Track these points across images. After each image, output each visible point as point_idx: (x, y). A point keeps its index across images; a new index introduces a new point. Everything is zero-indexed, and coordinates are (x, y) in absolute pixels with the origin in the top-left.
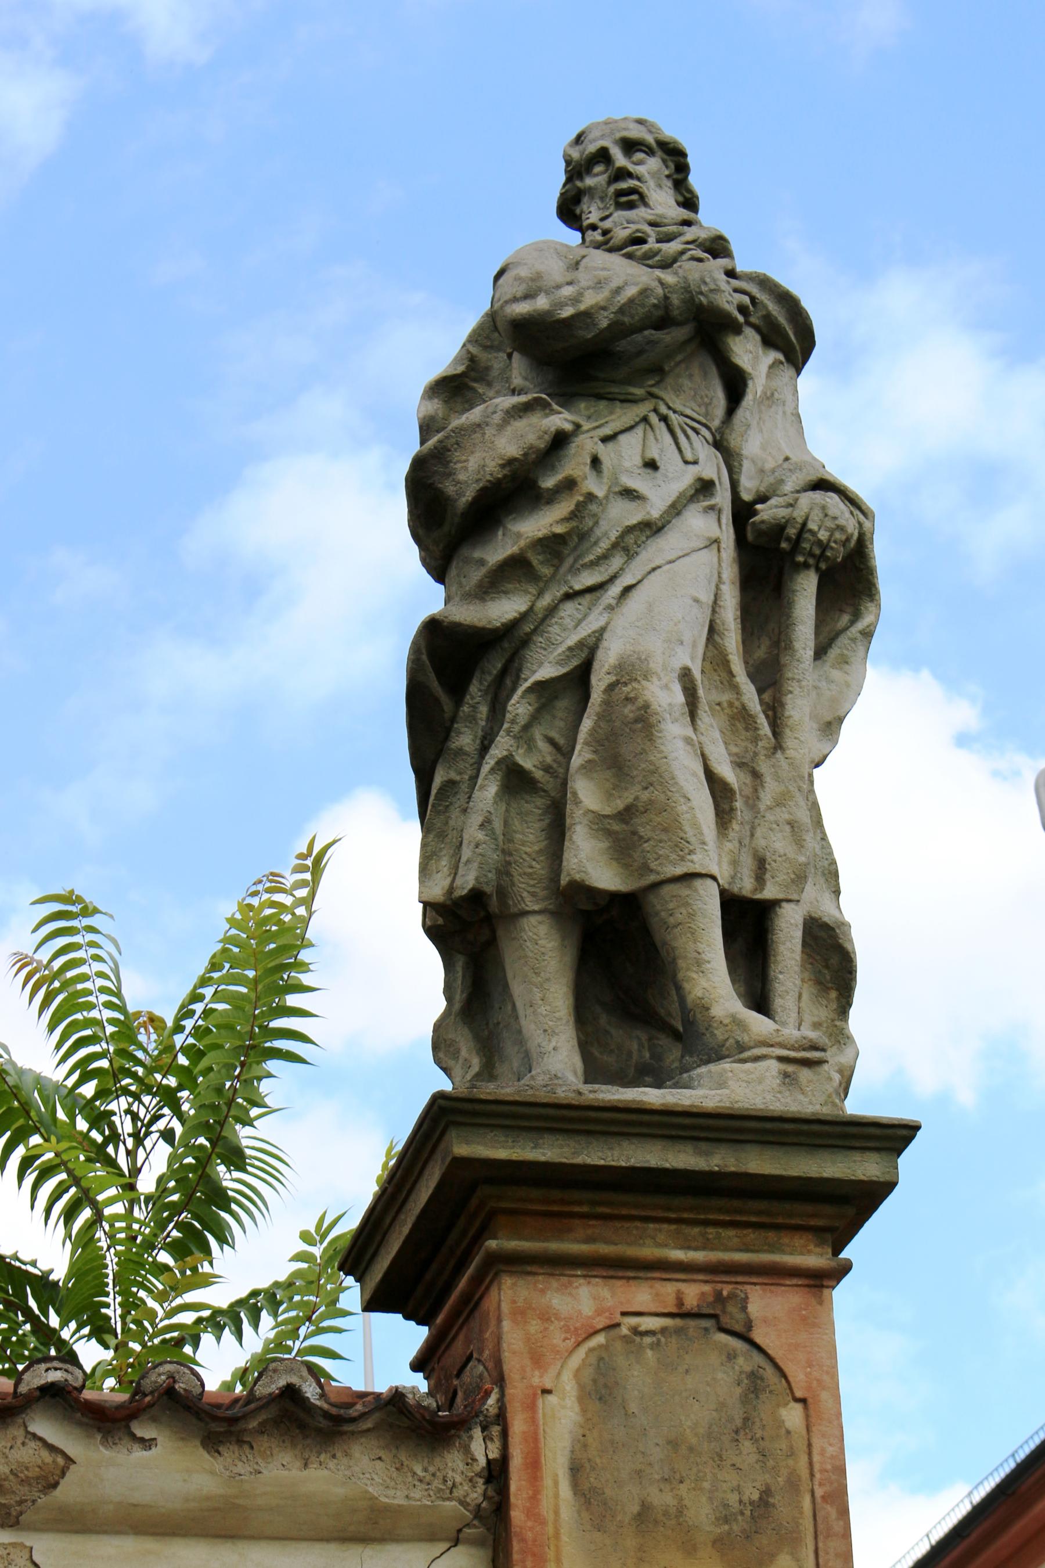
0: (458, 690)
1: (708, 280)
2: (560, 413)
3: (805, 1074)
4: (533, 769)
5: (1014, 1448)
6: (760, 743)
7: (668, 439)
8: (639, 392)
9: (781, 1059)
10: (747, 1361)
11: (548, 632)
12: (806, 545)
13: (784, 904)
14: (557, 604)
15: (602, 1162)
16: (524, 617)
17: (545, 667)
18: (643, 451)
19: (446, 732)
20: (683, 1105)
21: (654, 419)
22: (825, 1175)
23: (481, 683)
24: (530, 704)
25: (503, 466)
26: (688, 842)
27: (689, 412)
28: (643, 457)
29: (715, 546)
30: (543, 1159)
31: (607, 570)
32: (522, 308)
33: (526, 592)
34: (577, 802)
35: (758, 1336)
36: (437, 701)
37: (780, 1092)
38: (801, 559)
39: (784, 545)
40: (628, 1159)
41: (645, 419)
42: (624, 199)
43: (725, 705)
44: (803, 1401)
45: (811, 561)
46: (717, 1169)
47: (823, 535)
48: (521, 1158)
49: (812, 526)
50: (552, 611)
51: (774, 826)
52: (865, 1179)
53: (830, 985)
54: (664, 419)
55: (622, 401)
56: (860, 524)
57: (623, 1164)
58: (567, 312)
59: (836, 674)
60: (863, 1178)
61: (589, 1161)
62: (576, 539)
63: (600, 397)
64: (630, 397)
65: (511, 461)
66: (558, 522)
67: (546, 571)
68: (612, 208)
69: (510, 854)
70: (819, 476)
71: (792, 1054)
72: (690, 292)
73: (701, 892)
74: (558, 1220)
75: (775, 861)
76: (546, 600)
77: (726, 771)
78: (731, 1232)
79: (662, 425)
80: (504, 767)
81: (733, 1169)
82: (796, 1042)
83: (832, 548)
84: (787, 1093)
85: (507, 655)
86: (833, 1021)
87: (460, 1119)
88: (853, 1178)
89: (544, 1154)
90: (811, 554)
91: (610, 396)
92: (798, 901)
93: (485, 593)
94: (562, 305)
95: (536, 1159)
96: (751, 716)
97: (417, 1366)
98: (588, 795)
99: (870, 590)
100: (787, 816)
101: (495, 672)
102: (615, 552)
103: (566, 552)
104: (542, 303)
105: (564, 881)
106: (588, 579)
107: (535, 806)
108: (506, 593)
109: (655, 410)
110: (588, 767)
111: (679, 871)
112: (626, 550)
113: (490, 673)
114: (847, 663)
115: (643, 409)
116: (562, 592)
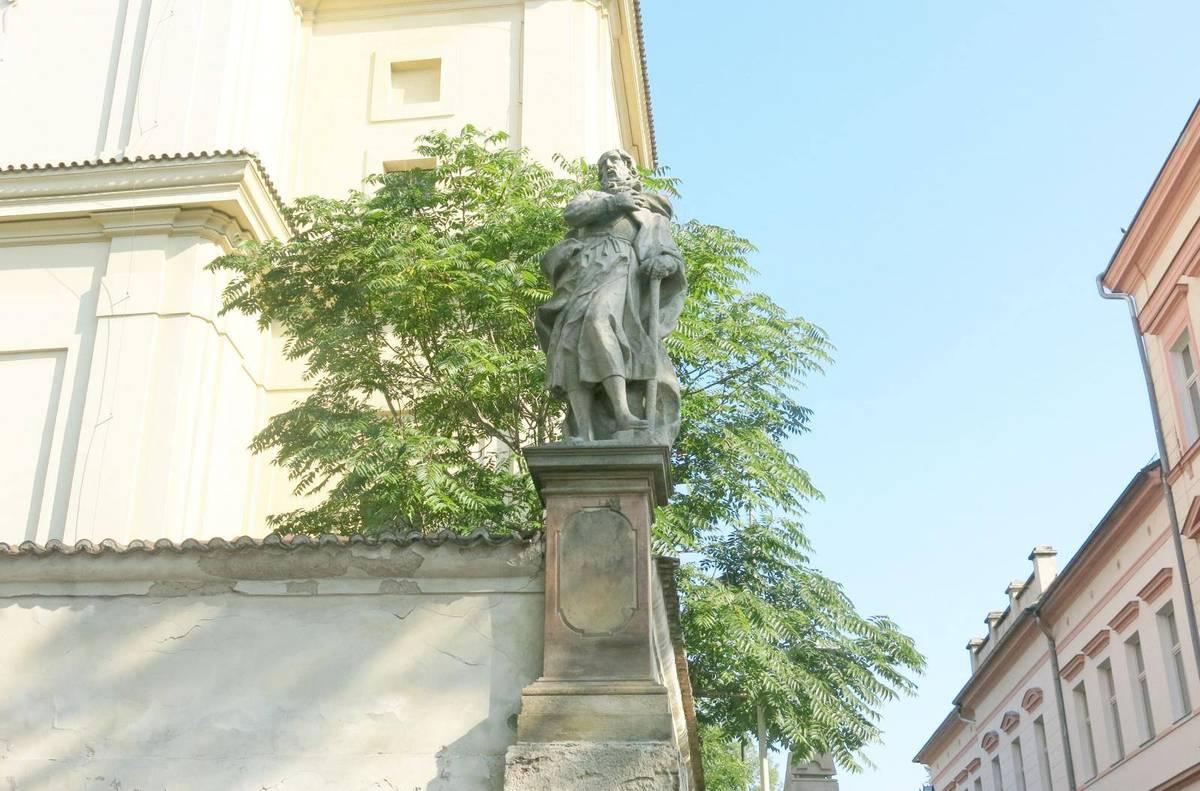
0: (551, 326)
5: (1149, 754)
10: (619, 518)
16: (566, 304)
19: (549, 339)
35: (622, 511)
41: (605, 242)
44: (636, 530)
47: (659, 269)
50: (575, 301)
54: (611, 240)
58: (578, 214)
59: (672, 308)
67: (571, 290)
74: (565, 481)
76: (571, 300)
78: (615, 482)
97: (836, 781)
104: (572, 211)
106: (585, 291)
115: (605, 238)
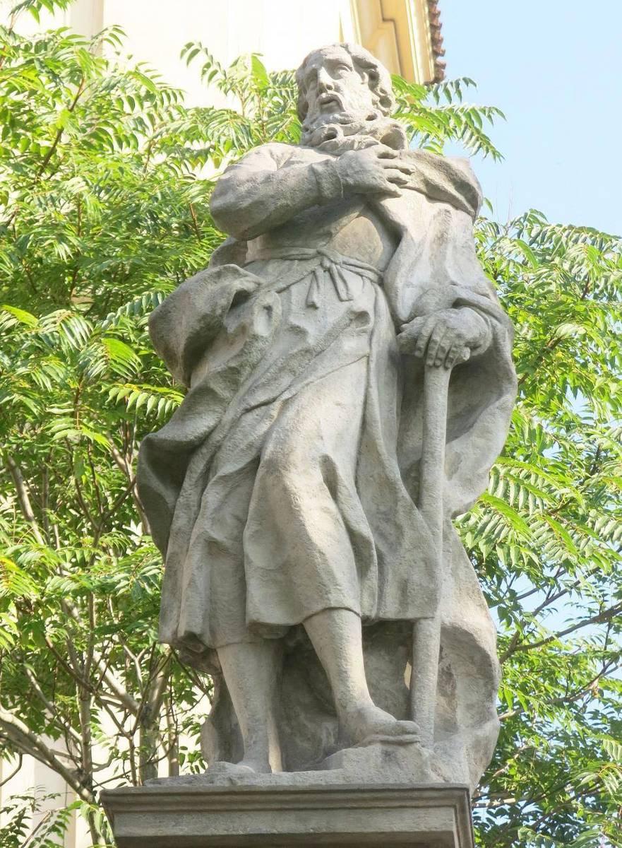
1: (353, 165)
2: (246, 276)
3: (401, 751)
4: (225, 540)
6: (399, 503)
7: (329, 285)
8: (311, 251)
9: (384, 742)
11: (234, 439)
12: (433, 353)
13: (422, 621)
14: (240, 417)
15: (225, 833)
17: (229, 466)
18: (308, 296)
20: (283, 786)
21: (320, 272)
22: (395, 830)
23: (190, 480)
24: (217, 493)
25: (199, 321)
26: (325, 585)
27: (352, 261)
28: (307, 301)
29: (365, 360)
30: (181, 833)
31: (277, 388)
32: (219, 203)
33: (214, 411)
34: (250, 562)
36: (160, 496)
37: (383, 768)
38: (430, 362)
39: (417, 354)
40: (245, 829)
42: (325, 106)
43: (376, 476)
45: (438, 363)
46: (312, 831)
48: (164, 834)
49: (437, 338)
50: (236, 422)
51: (413, 563)
52: (427, 830)
53: (478, 676)
54: (329, 270)
55: (300, 260)
56: (494, 328)
57: (241, 833)
58: (245, 204)
59: (480, 442)
60: (424, 829)
61: (216, 832)
62: (248, 369)
63: (284, 258)
64: (305, 256)
65: (205, 317)
66: (232, 358)
68: (318, 113)
69: (216, 603)
70: (457, 297)
71: (391, 738)
72: (337, 176)
73: (337, 621)
75: (414, 590)
76: (229, 416)
77: (365, 529)
79: (327, 274)
80: (202, 540)
81: (324, 830)
82: (393, 729)
83: (454, 352)
84: (387, 768)
85: (208, 456)
86: (483, 702)
87: (121, 809)
88: (417, 830)
89: (182, 830)
90: (437, 358)
91: (292, 257)
92: (433, 618)
93: (185, 415)
94: (242, 198)
95: (177, 834)
96: (392, 483)
98: (256, 555)
99: (508, 375)
100: (421, 555)
101: (199, 471)
102: (283, 374)
103: (242, 379)
105: (247, 622)
107: (226, 565)
108: (199, 414)
109: (321, 265)
110: (257, 536)
111: (320, 607)
112: (293, 372)
113: (196, 472)
114: (489, 432)
116: (241, 408)
